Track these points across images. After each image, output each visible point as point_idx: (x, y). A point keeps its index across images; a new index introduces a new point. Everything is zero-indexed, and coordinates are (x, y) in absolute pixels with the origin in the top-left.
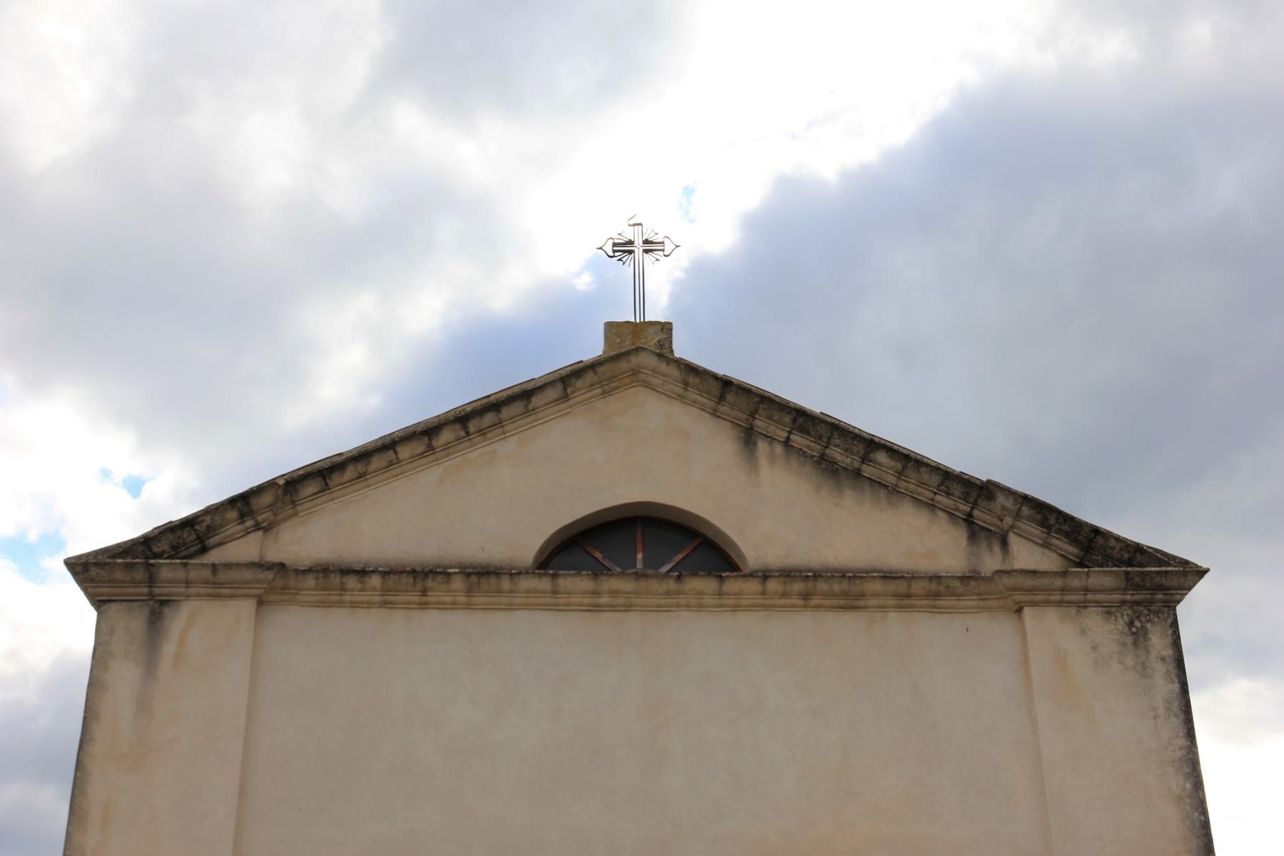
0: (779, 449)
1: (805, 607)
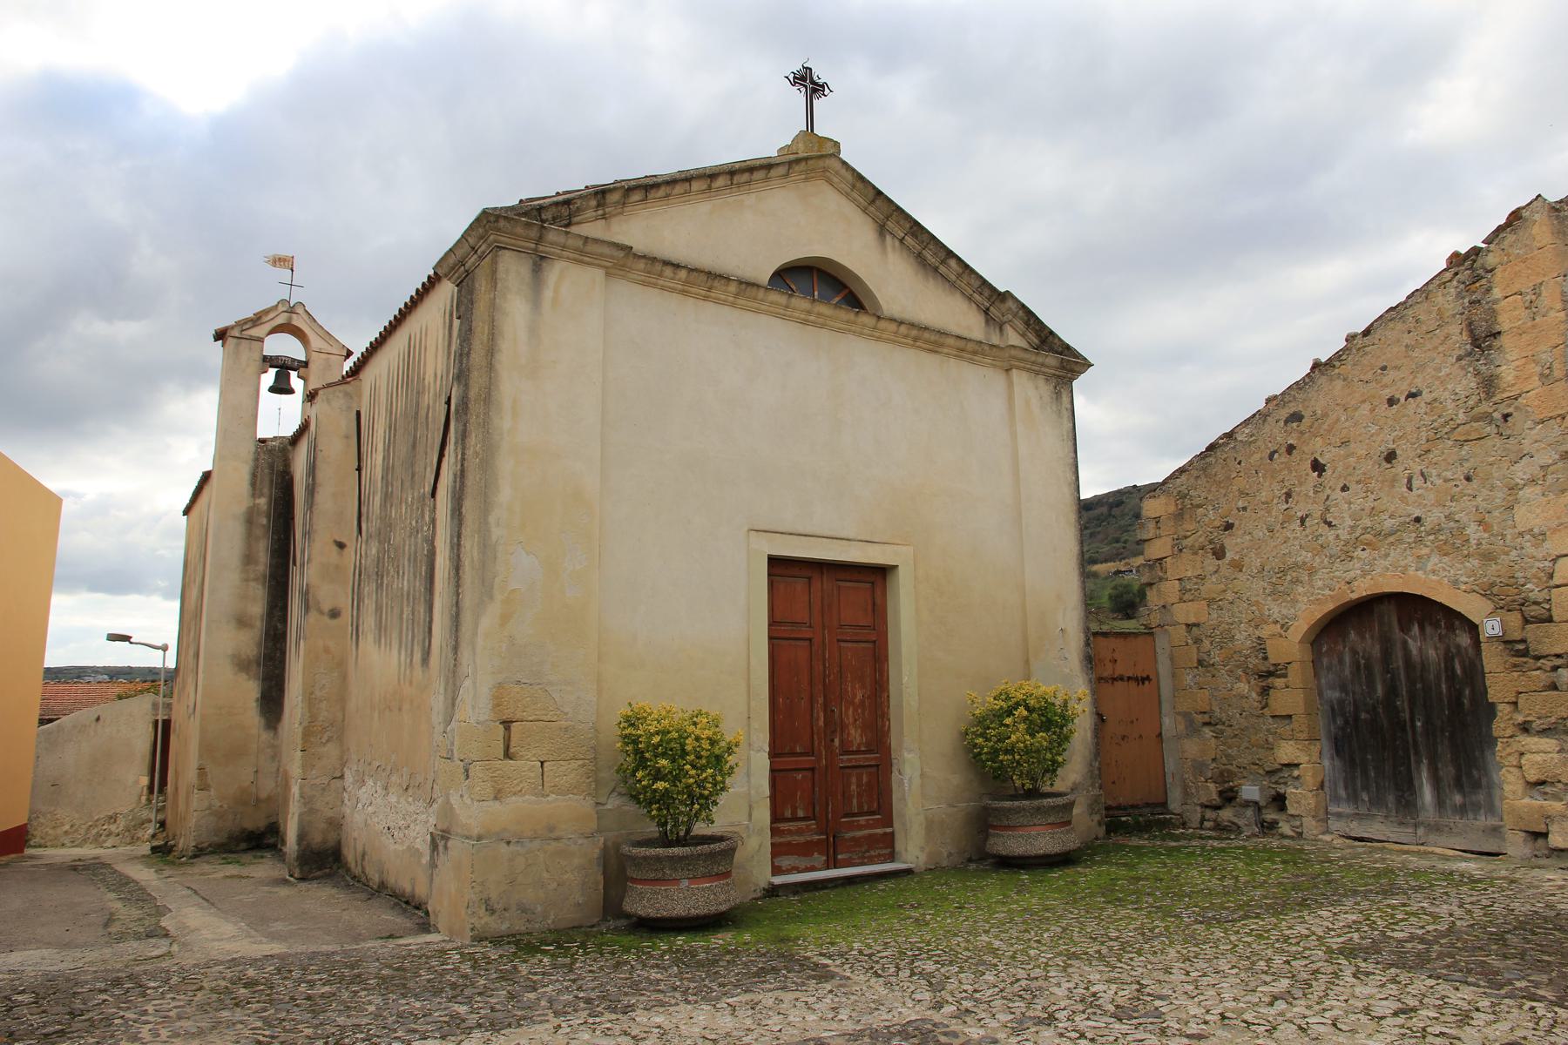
0: (897, 243)
1: (913, 346)
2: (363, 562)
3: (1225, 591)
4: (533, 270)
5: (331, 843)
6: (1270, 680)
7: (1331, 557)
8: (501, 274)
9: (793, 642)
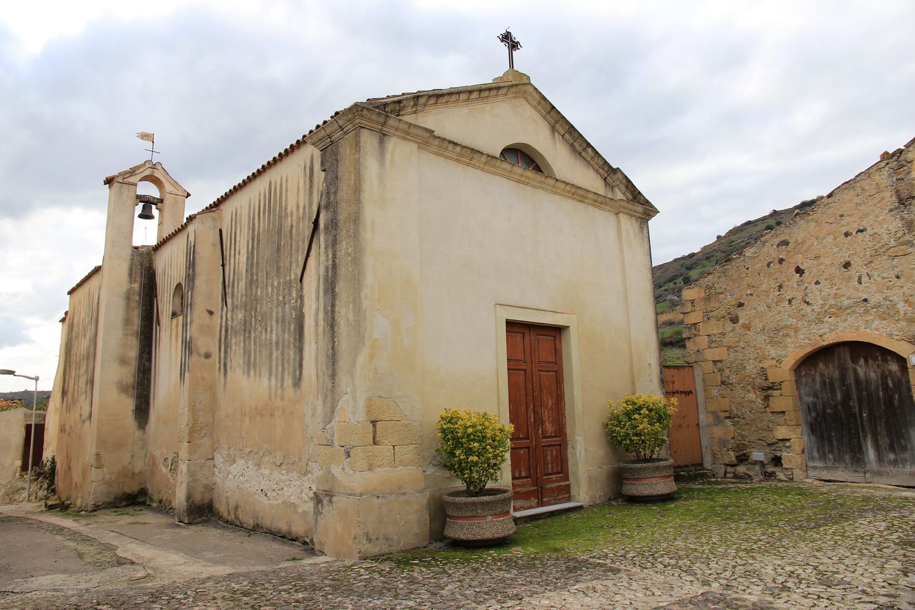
0: (561, 137)
2: (230, 323)
3: (739, 341)
4: (380, 142)
5: (207, 501)
6: (770, 392)
7: (809, 322)
8: (362, 144)
9: (516, 372)
